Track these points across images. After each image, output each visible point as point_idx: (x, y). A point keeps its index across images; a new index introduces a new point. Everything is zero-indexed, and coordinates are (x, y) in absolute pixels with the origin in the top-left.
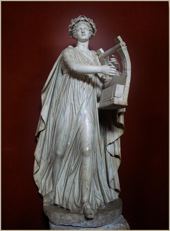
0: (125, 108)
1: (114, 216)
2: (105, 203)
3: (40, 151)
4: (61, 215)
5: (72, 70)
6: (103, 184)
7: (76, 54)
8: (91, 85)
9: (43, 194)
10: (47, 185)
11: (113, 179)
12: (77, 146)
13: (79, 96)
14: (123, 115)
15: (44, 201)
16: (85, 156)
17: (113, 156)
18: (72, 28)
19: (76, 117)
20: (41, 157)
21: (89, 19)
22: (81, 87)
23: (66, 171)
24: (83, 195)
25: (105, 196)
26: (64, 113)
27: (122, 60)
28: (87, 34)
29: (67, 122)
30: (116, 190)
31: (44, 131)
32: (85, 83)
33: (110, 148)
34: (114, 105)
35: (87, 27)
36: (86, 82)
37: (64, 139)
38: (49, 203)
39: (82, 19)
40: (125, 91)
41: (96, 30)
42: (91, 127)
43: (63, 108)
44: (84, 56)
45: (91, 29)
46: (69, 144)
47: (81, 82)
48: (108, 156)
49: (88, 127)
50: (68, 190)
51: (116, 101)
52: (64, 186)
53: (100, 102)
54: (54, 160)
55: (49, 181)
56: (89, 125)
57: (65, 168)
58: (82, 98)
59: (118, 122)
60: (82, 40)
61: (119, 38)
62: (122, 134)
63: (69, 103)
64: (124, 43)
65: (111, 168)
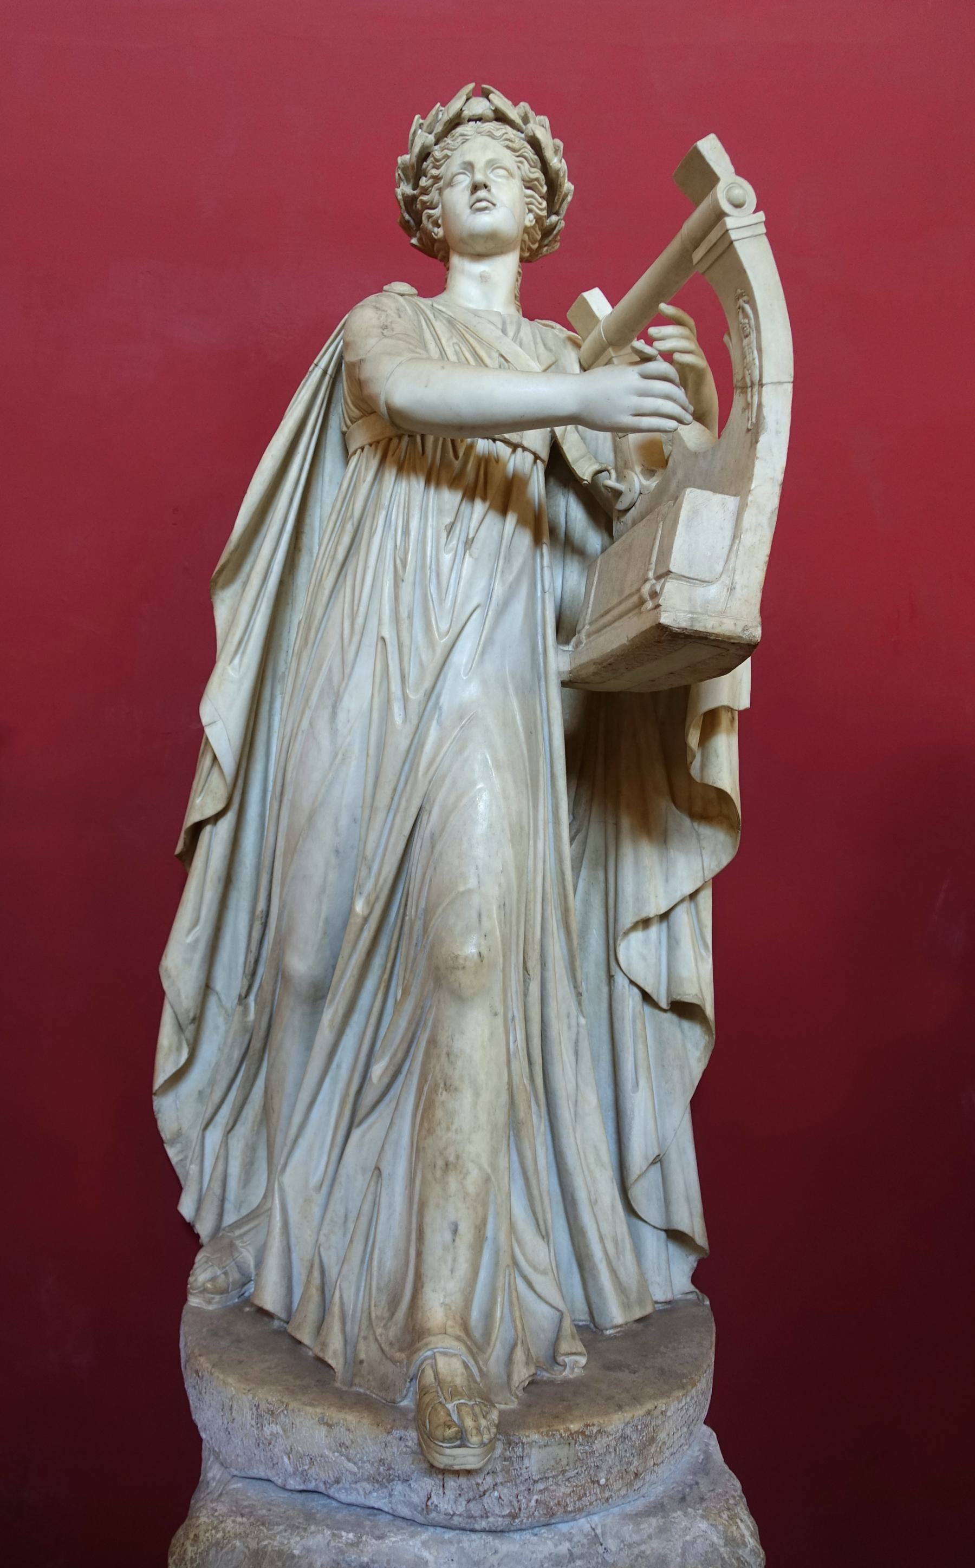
0: (749, 659)
1: (642, 1451)
2: (591, 1331)
3: (193, 946)
4: (263, 1406)
5: (389, 408)
6: (582, 1196)
7: (428, 320)
8: (521, 522)
9: (204, 1229)
10: (235, 1168)
11: (658, 1160)
12: (400, 927)
13: (433, 588)
14: (729, 732)
15: (191, 1279)
16: (459, 997)
17: (664, 1004)
18: (416, 173)
19: (409, 729)
20: (207, 988)
21: (522, 104)
22: (450, 529)
23: (341, 1085)
24: (428, 1271)
25: (596, 1278)
26: (334, 707)
27: (726, 329)
28: (508, 206)
29: (354, 763)
30: (675, 1236)
31: (225, 826)
32: (479, 507)
33: (640, 954)
34: (665, 638)
35: (509, 159)
36: (484, 499)
37: (332, 876)
38: (224, 1291)
39: (479, 106)
40: (748, 539)
41: (568, 186)
42: (506, 798)
43: (330, 670)
44: (480, 340)
45: (538, 174)
46: (360, 907)
47: (450, 498)
48: (630, 1001)
49: (482, 807)
50: (346, 1216)
51: (677, 609)
52: (324, 1190)
53: (574, 640)
54: (274, 1005)
55: (247, 1144)
56: (498, 803)
57: (338, 1066)
58: (448, 603)
59: (698, 780)
60: (474, 237)
61: (711, 148)
62: (725, 860)
63: (371, 638)
64: (746, 191)
65: (643, 1082)
